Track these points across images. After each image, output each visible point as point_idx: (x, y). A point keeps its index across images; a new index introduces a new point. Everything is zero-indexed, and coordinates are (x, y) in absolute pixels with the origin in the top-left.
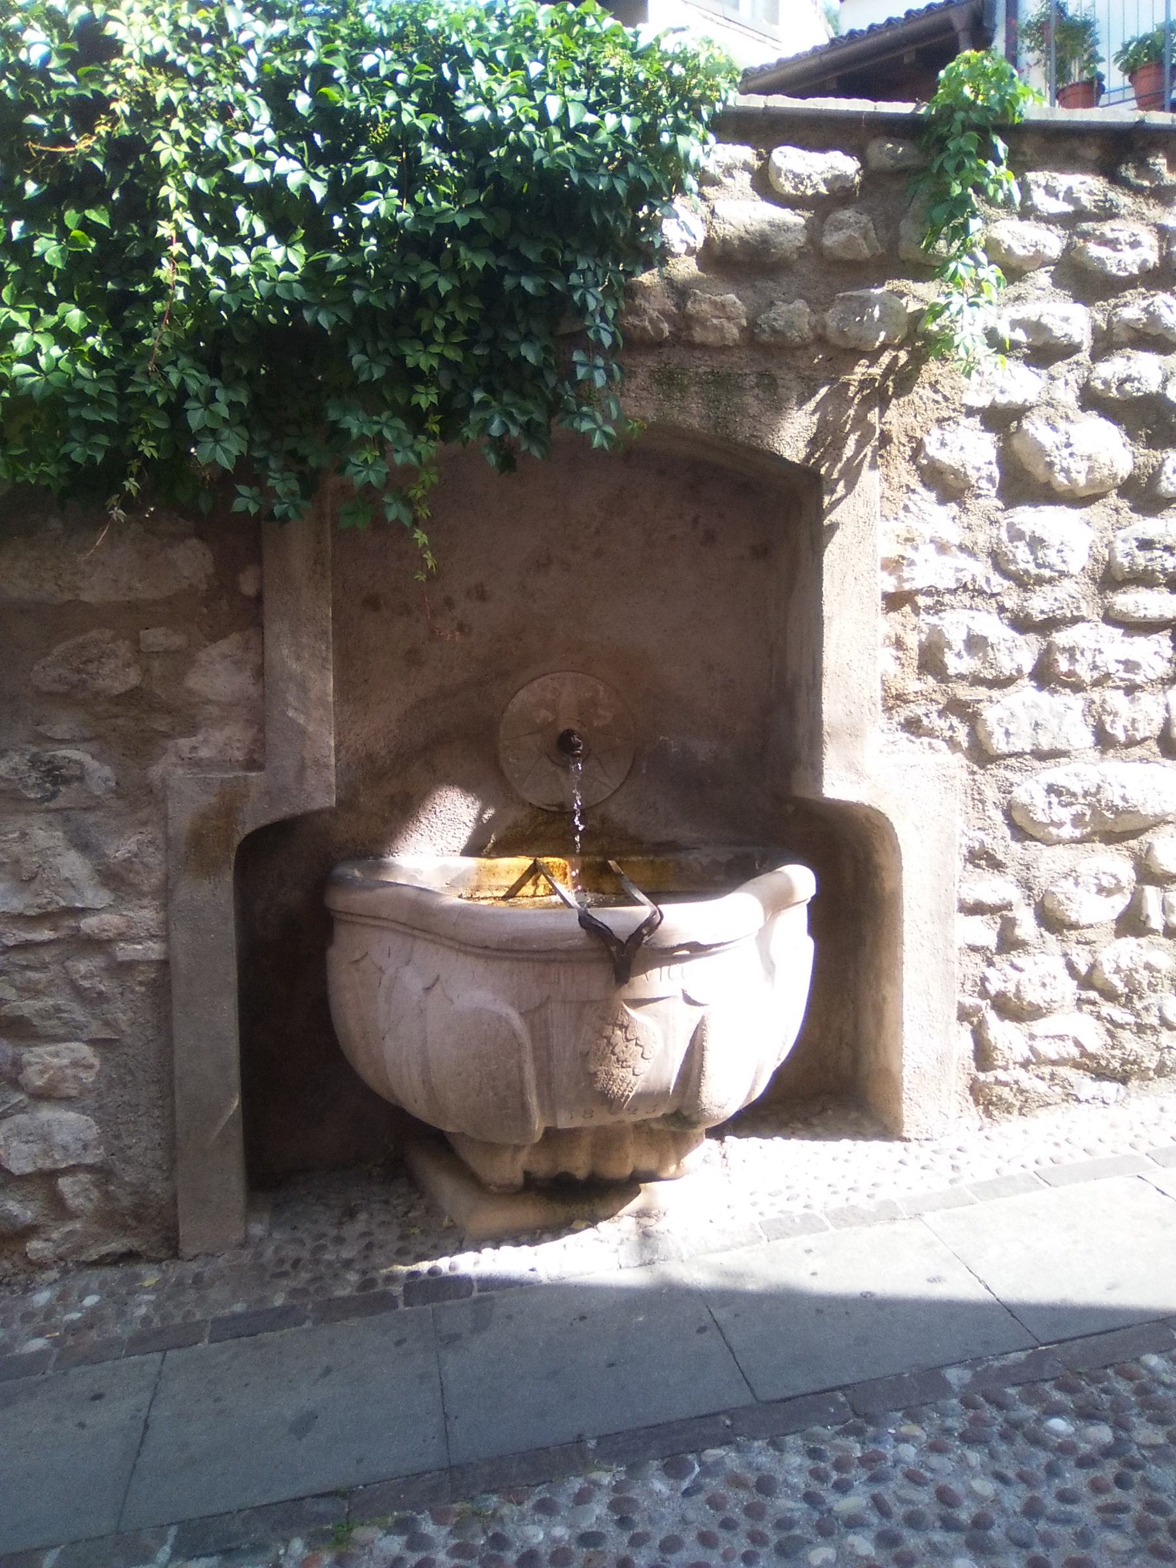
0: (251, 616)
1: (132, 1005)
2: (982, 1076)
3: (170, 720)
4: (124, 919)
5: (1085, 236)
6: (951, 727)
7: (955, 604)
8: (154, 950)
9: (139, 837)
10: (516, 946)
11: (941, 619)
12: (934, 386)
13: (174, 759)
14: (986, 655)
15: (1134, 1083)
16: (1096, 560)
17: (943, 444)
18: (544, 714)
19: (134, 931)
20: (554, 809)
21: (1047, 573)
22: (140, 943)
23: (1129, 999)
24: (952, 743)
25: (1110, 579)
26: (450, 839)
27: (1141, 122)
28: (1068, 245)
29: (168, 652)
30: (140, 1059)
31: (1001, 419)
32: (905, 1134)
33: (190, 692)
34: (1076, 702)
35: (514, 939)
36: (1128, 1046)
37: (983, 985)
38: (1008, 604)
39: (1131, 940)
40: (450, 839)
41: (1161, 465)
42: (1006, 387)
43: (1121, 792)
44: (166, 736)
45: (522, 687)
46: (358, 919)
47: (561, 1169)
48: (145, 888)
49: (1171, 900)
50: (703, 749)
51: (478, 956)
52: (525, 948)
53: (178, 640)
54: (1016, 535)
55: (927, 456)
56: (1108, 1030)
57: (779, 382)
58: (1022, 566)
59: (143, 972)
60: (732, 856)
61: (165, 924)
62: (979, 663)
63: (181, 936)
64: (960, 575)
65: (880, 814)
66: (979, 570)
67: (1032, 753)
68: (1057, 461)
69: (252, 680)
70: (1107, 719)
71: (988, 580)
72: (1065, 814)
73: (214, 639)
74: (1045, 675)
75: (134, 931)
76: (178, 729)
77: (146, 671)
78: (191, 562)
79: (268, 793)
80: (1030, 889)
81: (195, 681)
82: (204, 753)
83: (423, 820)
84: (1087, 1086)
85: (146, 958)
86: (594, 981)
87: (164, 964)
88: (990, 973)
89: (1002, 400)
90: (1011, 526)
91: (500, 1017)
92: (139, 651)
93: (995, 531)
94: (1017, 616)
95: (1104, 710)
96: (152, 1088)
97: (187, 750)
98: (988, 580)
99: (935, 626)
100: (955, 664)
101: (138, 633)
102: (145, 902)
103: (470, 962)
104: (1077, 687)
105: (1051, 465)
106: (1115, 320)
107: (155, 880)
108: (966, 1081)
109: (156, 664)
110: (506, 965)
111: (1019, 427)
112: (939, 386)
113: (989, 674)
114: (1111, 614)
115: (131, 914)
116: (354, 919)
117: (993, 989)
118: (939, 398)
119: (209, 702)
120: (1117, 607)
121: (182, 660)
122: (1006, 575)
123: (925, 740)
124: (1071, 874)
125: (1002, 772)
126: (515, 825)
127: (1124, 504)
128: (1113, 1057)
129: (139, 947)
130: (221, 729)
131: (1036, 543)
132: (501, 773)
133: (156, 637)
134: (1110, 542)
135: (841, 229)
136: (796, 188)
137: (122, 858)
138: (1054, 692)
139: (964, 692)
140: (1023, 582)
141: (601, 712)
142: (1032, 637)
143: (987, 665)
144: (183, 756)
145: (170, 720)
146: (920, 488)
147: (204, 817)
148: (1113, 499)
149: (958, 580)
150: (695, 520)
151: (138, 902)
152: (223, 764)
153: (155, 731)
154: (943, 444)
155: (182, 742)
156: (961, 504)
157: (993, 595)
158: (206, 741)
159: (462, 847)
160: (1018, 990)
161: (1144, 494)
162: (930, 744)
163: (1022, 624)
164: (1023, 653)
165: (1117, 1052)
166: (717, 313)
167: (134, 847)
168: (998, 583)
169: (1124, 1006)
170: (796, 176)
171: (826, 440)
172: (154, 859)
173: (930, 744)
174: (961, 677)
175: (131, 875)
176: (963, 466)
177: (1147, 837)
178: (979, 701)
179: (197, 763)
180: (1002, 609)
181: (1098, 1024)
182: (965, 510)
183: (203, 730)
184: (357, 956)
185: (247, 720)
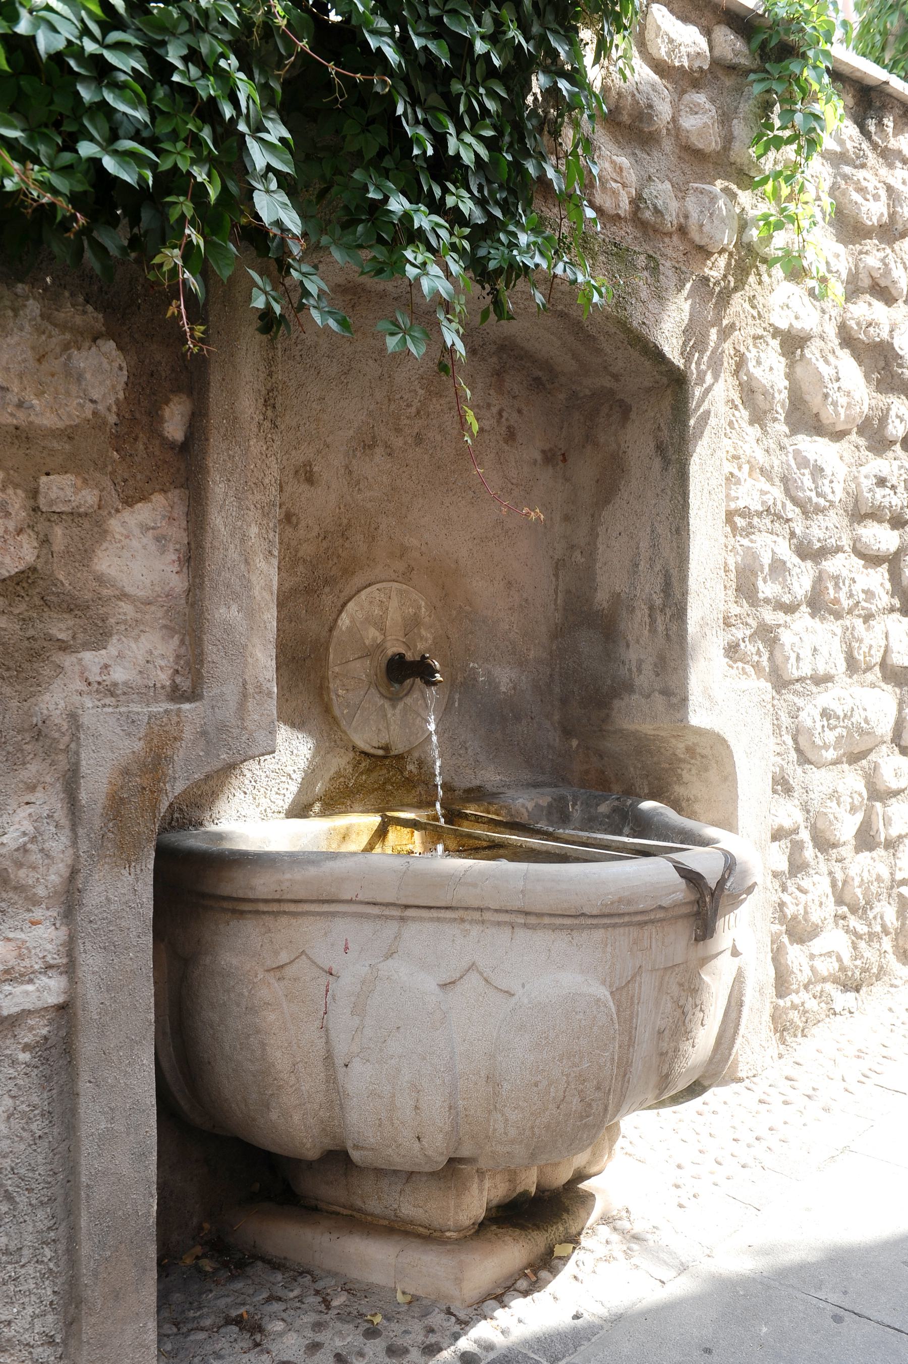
0: (184, 470)
1: (10, 1085)
2: (781, 1002)
3: (71, 623)
4: (11, 946)
5: (846, 177)
6: (758, 652)
7: (763, 528)
8: (50, 990)
9: (29, 810)
10: (623, 909)
11: (752, 541)
12: (752, 299)
13: (80, 686)
14: (785, 580)
15: (864, 989)
16: (848, 493)
17: (759, 363)
18: (372, 634)
19: (27, 963)
20: (381, 752)
21: (822, 501)
22: (31, 981)
23: (865, 911)
24: (757, 666)
25: (860, 513)
26: (274, 797)
27: (887, 83)
28: (834, 184)
29: (75, 515)
30: (22, 1171)
31: (793, 343)
32: (740, 1075)
33: (100, 579)
34: (837, 626)
35: (620, 901)
36: (865, 955)
37: (781, 911)
38: (798, 531)
39: (867, 854)
40: (274, 797)
41: (888, 409)
42: (800, 314)
43: (863, 714)
44: (64, 647)
45: (350, 599)
46: (263, 907)
47: (520, 1189)
48: (41, 891)
49: (890, 814)
50: (505, 677)
51: (555, 928)
52: (632, 909)
53: (88, 498)
54: (803, 462)
55: (748, 374)
56: (853, 942)
57: (661, 267)
58: (808, 493)
59: (31, 1029)
60: (550, 799)
61: (70, 947)
62: (780, 587)
63: (91, 961)
64: (765, 498)
65: (723, 742)
66: (777, 493)
67: (812, 678)
68: (831, 393)
69: (176, 568)
70: (856, 645)
71: (784, 505)
72: (830, 736)
73: (129, 502)
74: (817, 603)
75: (27, 963)
76: (80, 636)
77: (45, 541)
78: (102, 374)
79: (204, 733)
80: (808, 812)
81: (106, 562)
82: (119, 675)
83: (246, 772)
84: (843, 1000)
85: (39, 1005)
86: (676, 941)
87: (64, 1010)
88: (786, 898)
89: (798, 325)
90: (797, 453)
91: (599, 1000)
92: (36, 509)
93: (784, 458)
94: (801, 543)
95: (853, 637)
96: (41, 1214)
97: (96, 669)
98: (784, 505)
99: (748, 548)
100: (767, 589)
101: (36, 479)
102: (38, 913)
103: (541, 939)
104: (838, 616)
105: (826, 396)
106: (862, 265)
107: (55, 876)
108: (768, 1010)
109: (58, 533)
110: (598, 935)
111: (802, 355)
112: (755, 302)
113: (786, 599)
114: (858, 545)
115: (22, 936)
116: (263, 907)
117: (790, 911)
118: (756, 314)
119: (123, 596)
120: (863, 539)
121: (90, 525)
122: (795, 502)
123: (740, 664)
124: (835, 795)
125: (790, 697)
126: (338, 774)
127: (862, 442)
128: (856, 967)
129: (30, 988)
130: (137, 639)
131: (818, 471)
132: (327, 709)
133: (61, 489)
134: (855, 478)
135: (696, 113)
136: (668, 54)
137: (13, 846)
138: (823, 619)
139: (770, 616)
140: (808, 510)
141: (423, 632)
142: (809, 564)
143: (787, 590)
144: (91, 679)
145: (71, 623)
146: (741, 407)
147: (126, 772)
148: (854, 437)
149: (763, 503)
150: (500, 413)
151: (28, 915)
152: (147, 693)
153: (50, 638)
154: (759, 363)
155: (88, 656)
156: (763, 427)
157: (788, 520)
158: (120, 656)
159: (286, 807)
160: (806, 912)
161: (875, 434)
162: (743, 669)
163: (805, 551)
164: (802, 580)
165: (858, 962)
166: (614, 176)
167: (28, 826)
168: (792, 511)
169: (860, 918)
170: (671, 41)
171: (694, 335)
172: (58, 844)
173: (743, 669)
174: (767, 601)
175: (22, 873)
176: (772, 387)
177: (872, 757)
178: (779, 626)
179: (111, 691)
180: (793, 534)
181: (846, 936)
182: (765, 432)
183: (114, 639)
184: (284, 957)
185: (165, 627)
